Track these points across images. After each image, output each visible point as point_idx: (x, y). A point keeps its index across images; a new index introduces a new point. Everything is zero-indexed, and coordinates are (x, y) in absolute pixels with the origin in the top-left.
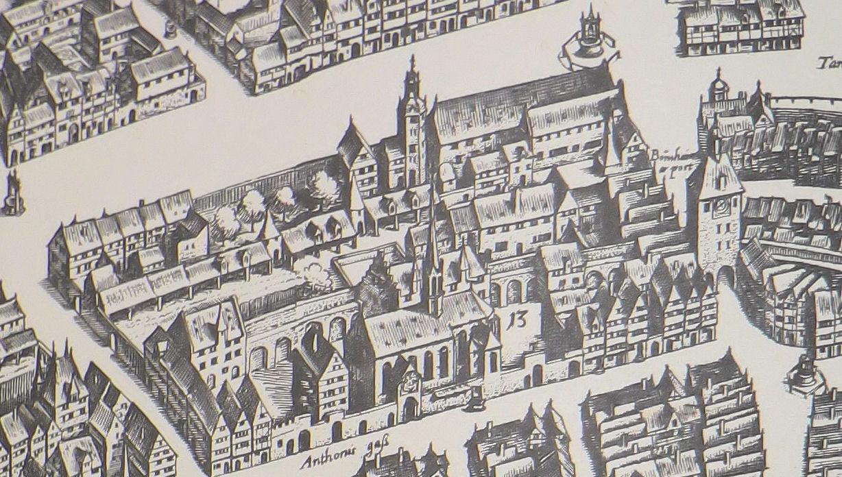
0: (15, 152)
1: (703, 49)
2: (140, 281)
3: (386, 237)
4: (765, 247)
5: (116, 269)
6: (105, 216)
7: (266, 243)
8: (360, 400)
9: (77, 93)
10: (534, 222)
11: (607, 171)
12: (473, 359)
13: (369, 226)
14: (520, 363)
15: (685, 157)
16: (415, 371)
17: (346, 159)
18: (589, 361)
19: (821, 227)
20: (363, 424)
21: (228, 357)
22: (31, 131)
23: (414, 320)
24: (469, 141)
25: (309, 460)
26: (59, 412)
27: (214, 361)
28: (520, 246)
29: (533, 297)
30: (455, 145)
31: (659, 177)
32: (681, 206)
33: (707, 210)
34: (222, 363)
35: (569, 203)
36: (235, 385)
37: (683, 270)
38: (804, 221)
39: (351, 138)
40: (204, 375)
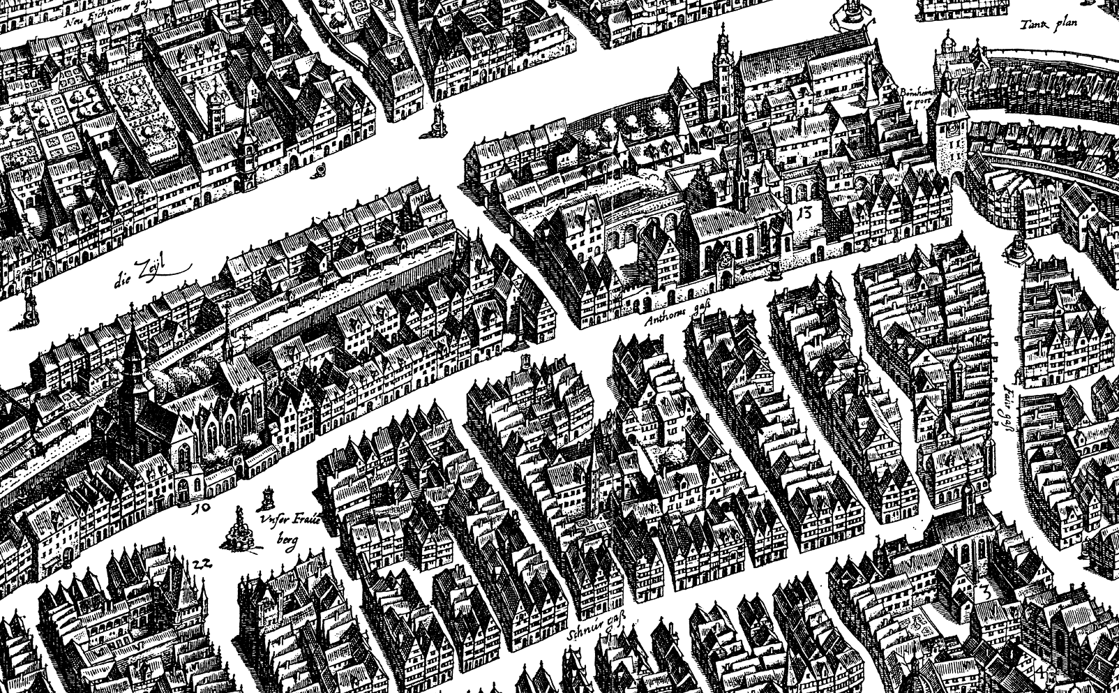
0: (440, 91)
1: (936, 16)
2: (531, 185)
3: (706, 154)
4: (986, 157)
5: (514, 177)
6: (506, 137)
7: (618, 155)
8: (689, 274)
9: (485, 48)
10: (815, 142)
11: (868, 104)
12: (772, 242)
13: (693, 147)
14: (807, 244)
15: (926, 93)
16: (729, 253)
17: (675, 98)
18: (858, 243)
19: (1026, 142)
20: (691, 291)
21: (592, 240)
22: (452, 75)
23: (727, 214)
24: (766, 84)
25: (651, 319)
26: (473, 281)
27: (582, 243)
28: (805, 160)
29: (816, 196)
30: (755, 87)
31: (906, 108)
32: (923, 128)
33: (942, 131)
34: (588, 245)
35: (841, 127)
36: (597, 260)
37: (927, 174)
38: (1014, 138)
39: (679, 84)
40: (576, 253)
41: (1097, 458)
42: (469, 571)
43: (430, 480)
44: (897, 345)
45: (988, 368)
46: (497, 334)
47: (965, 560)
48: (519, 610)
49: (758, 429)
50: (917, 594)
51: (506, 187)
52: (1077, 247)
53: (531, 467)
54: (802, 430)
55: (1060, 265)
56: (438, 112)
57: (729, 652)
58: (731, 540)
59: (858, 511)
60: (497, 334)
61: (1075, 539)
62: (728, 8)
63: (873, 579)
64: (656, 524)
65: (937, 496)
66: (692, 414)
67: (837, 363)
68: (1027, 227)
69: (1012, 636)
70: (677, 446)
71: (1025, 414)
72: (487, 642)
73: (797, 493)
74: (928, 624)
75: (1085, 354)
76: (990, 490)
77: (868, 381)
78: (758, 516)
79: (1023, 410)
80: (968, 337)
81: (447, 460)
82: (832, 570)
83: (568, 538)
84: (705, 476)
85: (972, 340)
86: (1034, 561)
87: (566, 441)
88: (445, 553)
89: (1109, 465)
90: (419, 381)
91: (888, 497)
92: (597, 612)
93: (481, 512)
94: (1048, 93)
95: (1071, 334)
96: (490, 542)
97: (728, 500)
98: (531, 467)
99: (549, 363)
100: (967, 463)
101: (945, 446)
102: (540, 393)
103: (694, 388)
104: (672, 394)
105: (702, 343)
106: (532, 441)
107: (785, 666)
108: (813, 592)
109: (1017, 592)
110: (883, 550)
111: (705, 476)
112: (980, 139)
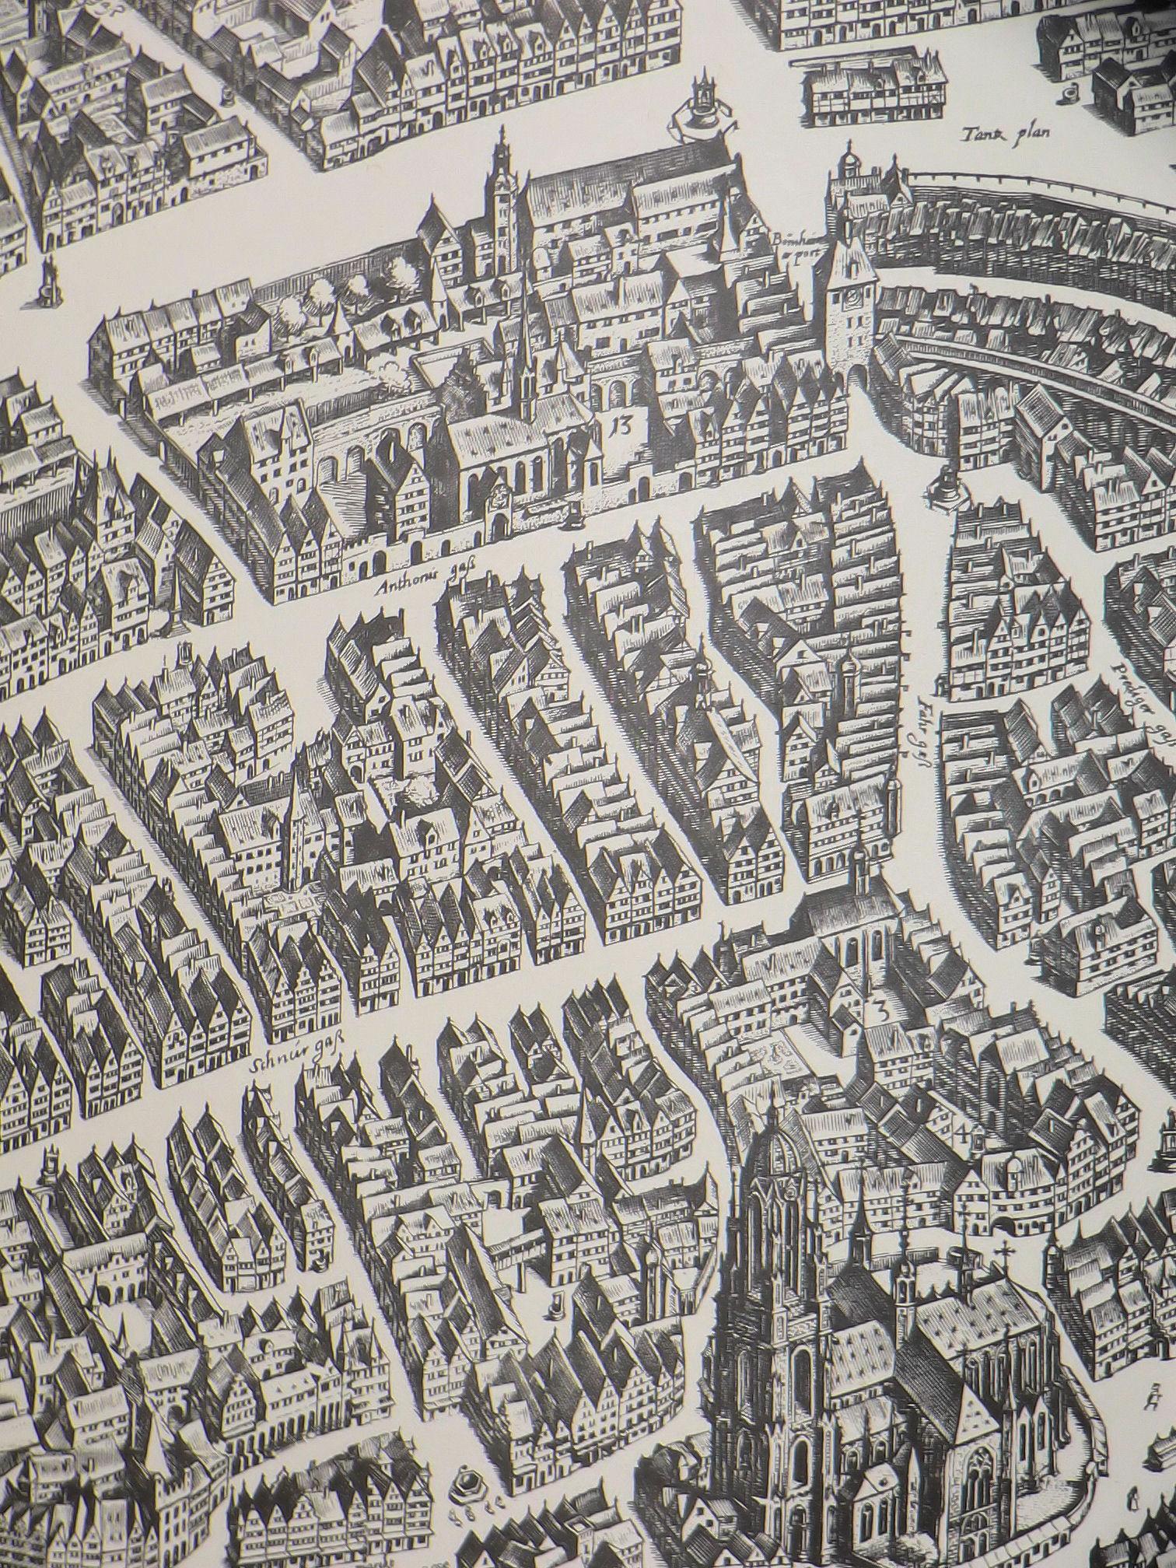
0: (51, 235)
1: (832, 118)
2: (193, 382)
3: (472, 331)
4: (903, 343)
5: (166, 368)
6: (153, 308)
7: (336, 338)
8: (442, 517)
10: (640, 315)
11: (723, 257)
12: (571, 470)
13: (453, 319)
14: (624, 475)
15: (811, 242)
16: (505, 484)
17: (426, 243)
18: (702, 473)
19: (965, 320)
20: (447, 544)
21: (293, 468)
22: (69, 212)
23: (504, 426)
24: (567, 224)
25: (385, 585)
26: (101, 531)
27: (277, 473)
28: (624, 342)
29: (638, 400)
30: (550, 228)
32: (806, 296)
33: (836, 301)
34: (285, 475)
35: (680, 293)
36: (301, 500)
37: (809, 369)
38: (946, 313)
39: (433, 220)
40: (266, 488)
41: (1054, 810)
42: (95, 967)
43: (37, 831)
44: (756, 632)
45: (895, 670)
46: (140, 610)
47: (852, 961)
48: (172, 1027)
49: (544, 759)
50: (778, 1011)
51: (156, 386)
52: (1038, 485)
53: (193, 813)
54: (611, 759)
55: (1005, 511)
56: (49, 269)
57: (495, 1091)
58: (501, 923)
59: (693, 885)
60: (140, 610)
61: (1020, 935)
62: (510, 103)
63: (713, 987)
64: (388, 897)
65: (812, 864)
66: (446, 731)
67: (667, 659)
68: (964, 452)
69: (920, 1078)
70: (422, 778)
71: (950, 741)
72: (123, 1074)
73: (601, 856)
74: (795, 1057)
75: (1045, 651)
76: (891, 855)
77: (712, 687)
78: (542, 888)
79: (946, 735)
80: (866, 621)
81: (62, 802)
82: (652, 973)
83: (252, 922)
84: (463, 829)
85: (871, 626)
86: (956, 966)
87: (251, 773)
88: (59, 941)
89: (1075, 822)
90: (20, 682)
91: (739, 864)
92: (298, 1032)
93: (114, 880)
94: (1002, 243)
95: (1024, 620)
96: (127, 925)
97: (498, 863)
98: (193, 813)
99: (221, 657)
100: (859, 816)
101: (828, 788)
102: (206, 702)
103: (450, 692)
104: (415, 699)
105: (461, 622)
106: (193, 773)
107: (579, 1113)
108: (623, 1006)
109: (929, 1011)
110: (728, 943)
111: (463, 829)
112: (892, 314)
